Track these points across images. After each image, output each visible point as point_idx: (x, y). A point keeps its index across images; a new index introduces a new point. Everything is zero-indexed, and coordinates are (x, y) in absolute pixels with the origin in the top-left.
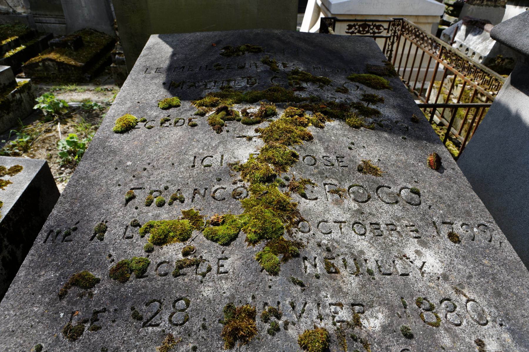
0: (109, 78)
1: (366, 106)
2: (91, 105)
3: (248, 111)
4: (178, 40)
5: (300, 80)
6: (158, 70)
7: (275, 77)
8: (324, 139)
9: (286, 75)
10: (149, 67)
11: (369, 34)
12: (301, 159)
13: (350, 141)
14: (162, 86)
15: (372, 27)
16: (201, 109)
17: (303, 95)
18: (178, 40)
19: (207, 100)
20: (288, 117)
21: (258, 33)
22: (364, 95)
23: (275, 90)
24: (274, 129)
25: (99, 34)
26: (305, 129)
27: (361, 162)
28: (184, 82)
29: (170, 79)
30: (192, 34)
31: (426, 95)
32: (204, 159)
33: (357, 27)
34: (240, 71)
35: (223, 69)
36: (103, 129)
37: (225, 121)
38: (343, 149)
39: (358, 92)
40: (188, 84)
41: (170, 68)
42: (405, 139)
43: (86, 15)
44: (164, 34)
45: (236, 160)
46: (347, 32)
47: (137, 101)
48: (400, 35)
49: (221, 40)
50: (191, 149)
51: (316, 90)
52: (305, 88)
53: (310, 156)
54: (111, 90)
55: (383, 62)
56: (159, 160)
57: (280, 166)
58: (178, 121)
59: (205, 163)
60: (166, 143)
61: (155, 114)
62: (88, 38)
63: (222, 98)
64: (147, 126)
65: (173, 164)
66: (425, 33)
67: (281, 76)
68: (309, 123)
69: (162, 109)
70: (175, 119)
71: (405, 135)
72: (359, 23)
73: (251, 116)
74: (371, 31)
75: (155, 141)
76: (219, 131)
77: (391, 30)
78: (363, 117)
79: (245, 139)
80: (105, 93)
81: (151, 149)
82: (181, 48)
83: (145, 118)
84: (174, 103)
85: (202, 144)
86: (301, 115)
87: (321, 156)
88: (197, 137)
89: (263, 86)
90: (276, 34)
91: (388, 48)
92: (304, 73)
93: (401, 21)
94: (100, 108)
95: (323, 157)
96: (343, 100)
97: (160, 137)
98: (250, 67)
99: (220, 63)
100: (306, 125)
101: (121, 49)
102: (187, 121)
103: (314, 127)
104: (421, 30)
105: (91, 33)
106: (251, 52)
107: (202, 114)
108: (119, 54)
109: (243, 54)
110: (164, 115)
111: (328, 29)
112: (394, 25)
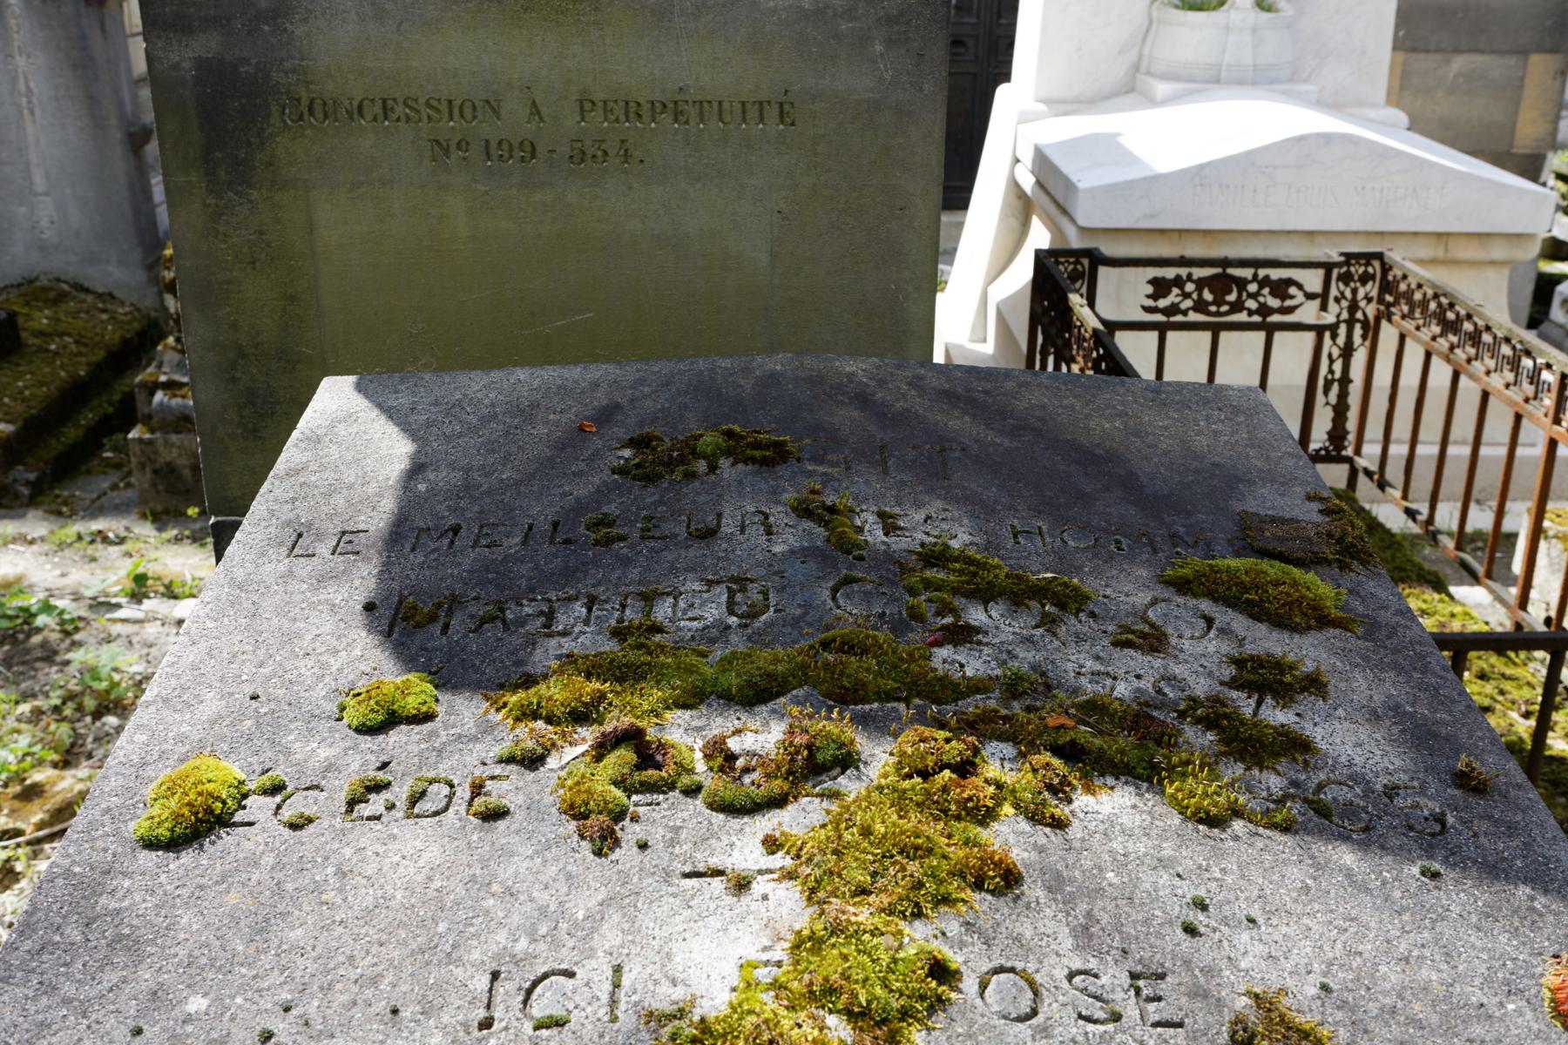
0: (114, 487)
1: (1247, 711)
2: (26, 610)
3: (734, 744)
4: (436, 404)
5: (956, 591)
6: (346, 543)
7: (849, 581)
8: (1072, 880)
9: (896, 568)
10: (310, 525)
11: (1242, 317)
12: (970, 984)
13: (1188, 890)
14: (359, 617)
15: (1253, 288)
16: (527, 735)
17: (975, 665)
18: (436, 404)
19: (555, 692)
20: (909, 776)
21: (773, 375)
22: (1239, 662)
23: (848, 647)
24: (847, 837)
25: (90, 298)
26: (983, 834)
27: (1245, 1000)
28: (455, 602)
29: (396, 585)
30: (496, 375)
31: (1518, 566)
32: (535, 984)
33: (1190, 287)
34: (695, 551)
35: (622, 538)
36: (92, 825)
37: (630, 791)
38: (1159, 935)
39: (1214, 646)
40: (473, 608)
41: (400, 534)
42: (1435, 875)
43: (44, 223)
44: (378, 370)
45: (679, 993)
46: (1147, 309)
47: (249, 690)
48: (1378, 319)
49: (618, 406)
50: (476, 936)
51: (1029, 640)
52: (978, 630)
53: (1012, 970)
54: (121, 541)
55: (1309, 498)
56: (330, 986)
57: (879, 1024)
58: (423, 794)
59: (542, 1006)
60: (370, 901)
61: (324, 753)
62: (42, 320)
63: (621, 680)
64: (287, 813)
65: (395, 1012)
66: (1481, 316)
67: (873, 576)
68: (999, 805)
69: (358, 730)
70: (410, 782)
71: (1431, 857)
72: (1199, 273)
73: (747, 770)
74: (1251, 304)
75: (317, 888)
76: (605, 842)
77: (1337, 300)
78: (1239, 769)
79: (717, 883)
80: (90, 550)
81: (299, 932)
82: (448, 438)
83: (279, 773)
84: (411, 704)
85: (528, 907)
86: (965, 769)
87: (1060, 974)
88: (506, 872)
89: (796, 622)
90: (851, 376)
91: (1331, 371)
92: (970, 561)
93: (1377, 264)
94: (62, 623)
95: (1071, 976)
96: (1146, 684)
97: (341, 874)
98: (743, 529)
99: (612, 509)
100: (985, 816)
101: (180, 366)
102: (463, 792)
103: (1024, 825)
104: (1465, 305)
105: (61, 297)
106: (745, 462)
107: (532, 762)
108: (170, 386)
109: (713, 468)
110: (361, 758)
111: (1066, 299)
112: (1346, 278)
